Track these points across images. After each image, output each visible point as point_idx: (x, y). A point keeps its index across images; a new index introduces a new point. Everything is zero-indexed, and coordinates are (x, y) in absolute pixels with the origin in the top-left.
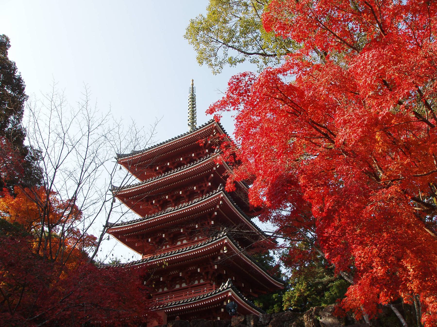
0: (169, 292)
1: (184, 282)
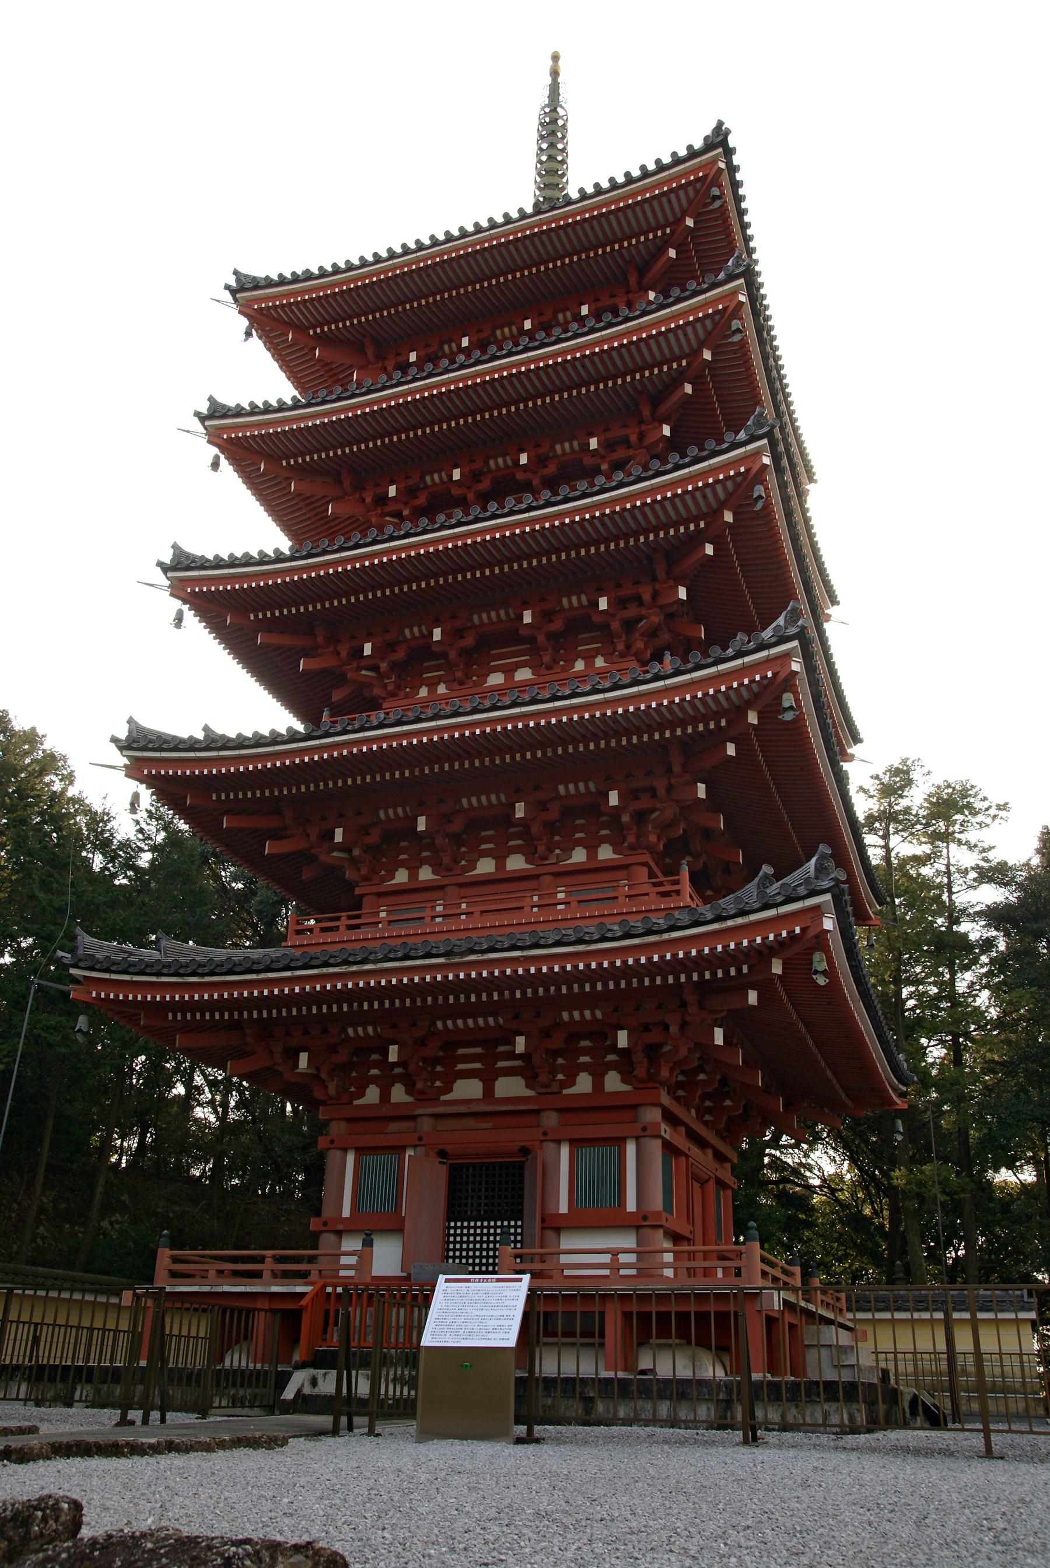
0: (441, 888)
1: (515, 850)
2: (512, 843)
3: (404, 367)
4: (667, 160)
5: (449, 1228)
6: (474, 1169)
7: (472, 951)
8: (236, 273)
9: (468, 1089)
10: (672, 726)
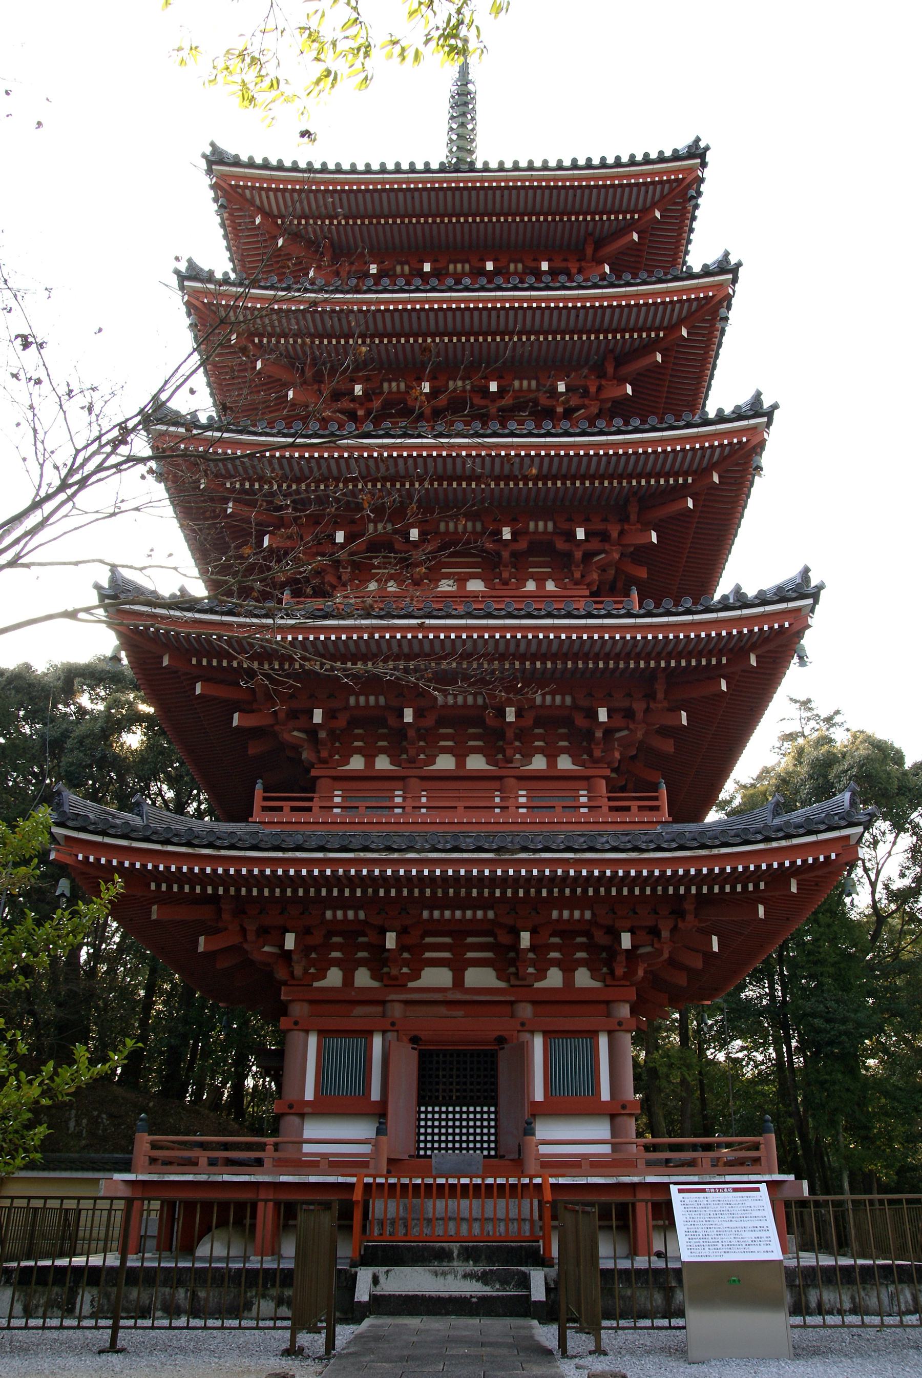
2: (471, 743)
3: (538, 274)
4: (654, 156)
5: (420, 1112)
6: (445, 1056)
7: (525, 849)
8: (213, 144)
9: (437, 977)
10: (689, 656)
